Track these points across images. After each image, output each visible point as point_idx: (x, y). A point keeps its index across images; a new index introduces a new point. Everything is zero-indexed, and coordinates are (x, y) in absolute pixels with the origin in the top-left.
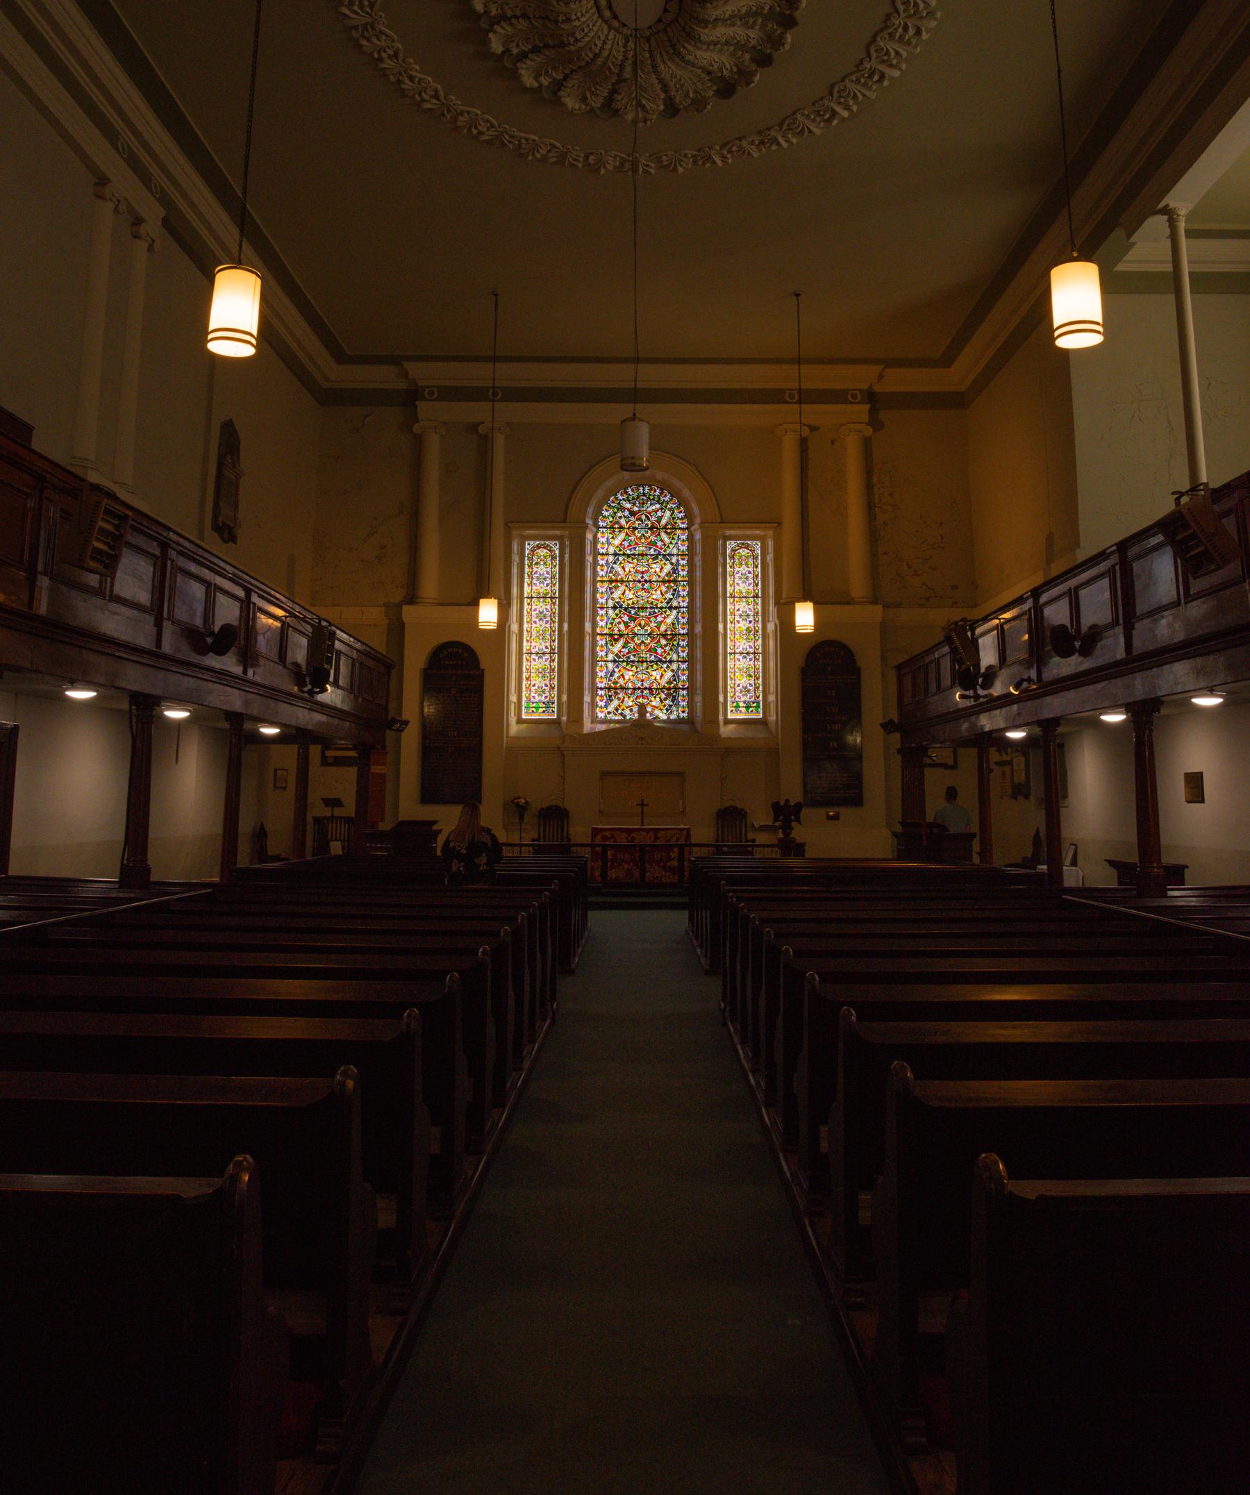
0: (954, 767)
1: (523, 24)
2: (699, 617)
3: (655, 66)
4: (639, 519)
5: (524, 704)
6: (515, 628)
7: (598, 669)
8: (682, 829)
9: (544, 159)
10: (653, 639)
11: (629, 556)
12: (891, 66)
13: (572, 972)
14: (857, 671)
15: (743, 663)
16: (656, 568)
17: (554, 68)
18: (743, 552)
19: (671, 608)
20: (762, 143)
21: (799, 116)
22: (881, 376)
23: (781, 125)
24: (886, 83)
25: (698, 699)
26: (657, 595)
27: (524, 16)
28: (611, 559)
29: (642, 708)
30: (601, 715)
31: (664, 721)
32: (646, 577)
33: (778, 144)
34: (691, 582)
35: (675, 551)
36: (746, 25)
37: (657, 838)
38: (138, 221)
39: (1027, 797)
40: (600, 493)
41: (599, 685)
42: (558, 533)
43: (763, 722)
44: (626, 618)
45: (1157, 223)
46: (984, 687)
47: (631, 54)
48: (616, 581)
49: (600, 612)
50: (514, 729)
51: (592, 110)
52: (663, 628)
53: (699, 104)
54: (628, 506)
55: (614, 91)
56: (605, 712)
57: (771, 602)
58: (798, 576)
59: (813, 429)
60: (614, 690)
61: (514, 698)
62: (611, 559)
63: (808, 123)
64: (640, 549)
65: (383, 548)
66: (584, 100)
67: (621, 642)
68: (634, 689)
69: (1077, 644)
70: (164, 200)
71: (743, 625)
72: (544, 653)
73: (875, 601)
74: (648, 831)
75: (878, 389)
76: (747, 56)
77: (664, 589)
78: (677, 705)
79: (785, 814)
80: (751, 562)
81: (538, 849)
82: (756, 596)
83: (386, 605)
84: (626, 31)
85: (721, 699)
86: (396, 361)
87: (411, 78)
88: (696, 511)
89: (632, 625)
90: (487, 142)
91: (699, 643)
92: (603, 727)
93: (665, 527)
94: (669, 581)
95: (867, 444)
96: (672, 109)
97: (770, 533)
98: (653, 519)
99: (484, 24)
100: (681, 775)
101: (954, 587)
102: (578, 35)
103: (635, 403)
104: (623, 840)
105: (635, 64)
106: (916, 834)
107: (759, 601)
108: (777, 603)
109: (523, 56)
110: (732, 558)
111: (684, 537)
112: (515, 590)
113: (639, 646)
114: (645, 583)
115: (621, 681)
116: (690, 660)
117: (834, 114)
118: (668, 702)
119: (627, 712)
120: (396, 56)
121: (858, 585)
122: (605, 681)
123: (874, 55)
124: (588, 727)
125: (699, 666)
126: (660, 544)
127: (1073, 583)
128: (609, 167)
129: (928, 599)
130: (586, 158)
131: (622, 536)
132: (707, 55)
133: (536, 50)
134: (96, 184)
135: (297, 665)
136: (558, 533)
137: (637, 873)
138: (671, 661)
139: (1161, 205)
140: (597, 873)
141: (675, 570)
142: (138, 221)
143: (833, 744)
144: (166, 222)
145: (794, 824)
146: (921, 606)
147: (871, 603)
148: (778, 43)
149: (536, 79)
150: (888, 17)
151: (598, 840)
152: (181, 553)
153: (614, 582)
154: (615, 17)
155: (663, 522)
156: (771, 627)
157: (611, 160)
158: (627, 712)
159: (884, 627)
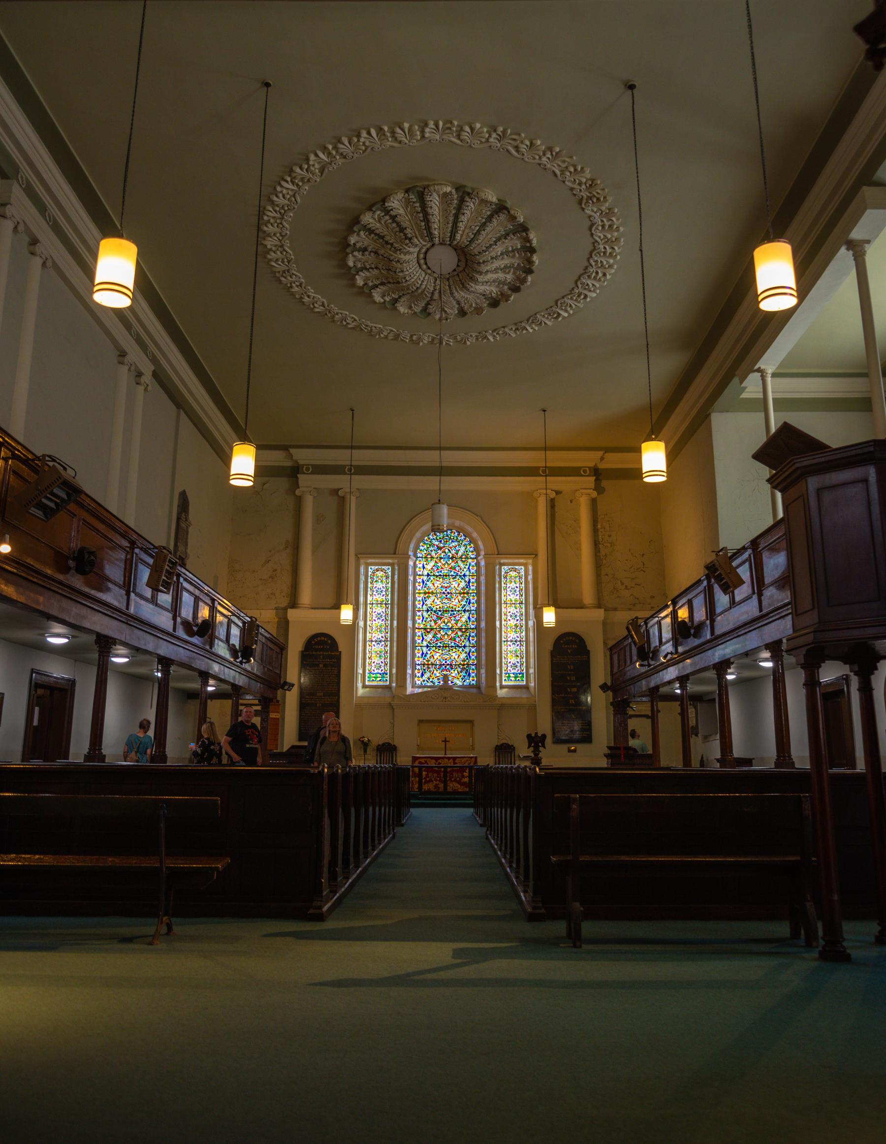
1: (376, 272)
2: (483, 616)
3: (452, 294)
4: (444, 552)
6: (361, 624)
9: (386, 337)
10: (453, 631)
12: (590, 291)
13: (402, 825)
15: (513, 648)
16: (455, 584)
17: (393, 292)
18: (513, 574)
20: (517, 329)
21: (538, 316)
22: (602, 459)
23: (528, 320)
24: (588, 299)
25: (483, 671)
27: (376, 268)
28: (425, 578)
29: (446, 678)
30: (418, 682)
31: (460, 686)
34: (478, 594)
36: (504, 272)
38: (139, 375)
40: (418, 535)
41: (417, 662)
42: (390, 561)
43: (526, 687)
45: (754, 377)
46: (652, 659)
47: (438, 287)
48: (429, 593)
49: (418, 614)
50: (361, 691)
51: (415, 313)
52: (459, 625)
53: (479, 310)
54: (437, 543)
55: (428, 304)
56: (419, 682)
57: (531, 607)
58: (553, 589)
59: (558, 493)
60: (427, 666)
61: (360, 671)
63: (544, 319)
64: (445, 572)
65: (275, 570)
66: (410, 308)
67: (432, 633)
68: (441, 665)
69: (692, 631)
70: (154, 360)
71: (513, 622)
73: (599, 606)
74: (449, 758)
75: (601, 466)
76: (506, 287)
77: (460, 598)
78: (469, 675)
79: (536, 741)
83: (276, 609)
84: (435, 275)
85: (498, 671)
86: (285, 448)
87: (309, 296)
88: (482, 547)
89: (439, 622)
90: (353, 328)
91: (483, 634)
92: (420, 690)
93: (461, 557)
94: (464, 593)
95: (594, 503)
96: (462, 313)
97: (530, 561)
98: (453, 552)
99: (353, 271)
101: (652, 597)
102: (407, 278)
103: (440, 475)
104: (432, 763)
105: (440, 292)
106: (620, 752)
107: (523, 606)
108: (535, 608)
109: (375, 287)
110: (505, 578)
111: (473, 564)
112: (362, 599)
113: (444, 636)
114: (447, 594)
115: (432, 660)
116: (478, 646)
117: (559, 315)
118: (463, 674)
119: (436, 680)
120: (301, 285)
121: (588, 595)
122: (421, 659)
123: (580, 286)
124: (409, 690)
125: (483, 650)
126: (457, 569)
127: (690, 596)
129: (634, 605)
130: (411, 336)
131: (432, 563)
132: (482, 288)
133: (383, 284)
134: (120, 356)
135: (234, 645)
136: (390, 561)
137: (441, 785)
138: (465, 646)
139: (756, 367)
140: (416, 786)
141: (468, 586)
142: (139, 375)
143: (572, 701)
144: (155, 375)
145: (541, 749)
146: (630, 609)
147: (595, 607)
148: (524, 281)
149: (382, 297)
151: (416, 764)
152: (185, 580)
154: (429, 268)
155: (460, 554)
156: (531, 623)
157: (426, 338)
158: (436, 680)
159: (605, 624)
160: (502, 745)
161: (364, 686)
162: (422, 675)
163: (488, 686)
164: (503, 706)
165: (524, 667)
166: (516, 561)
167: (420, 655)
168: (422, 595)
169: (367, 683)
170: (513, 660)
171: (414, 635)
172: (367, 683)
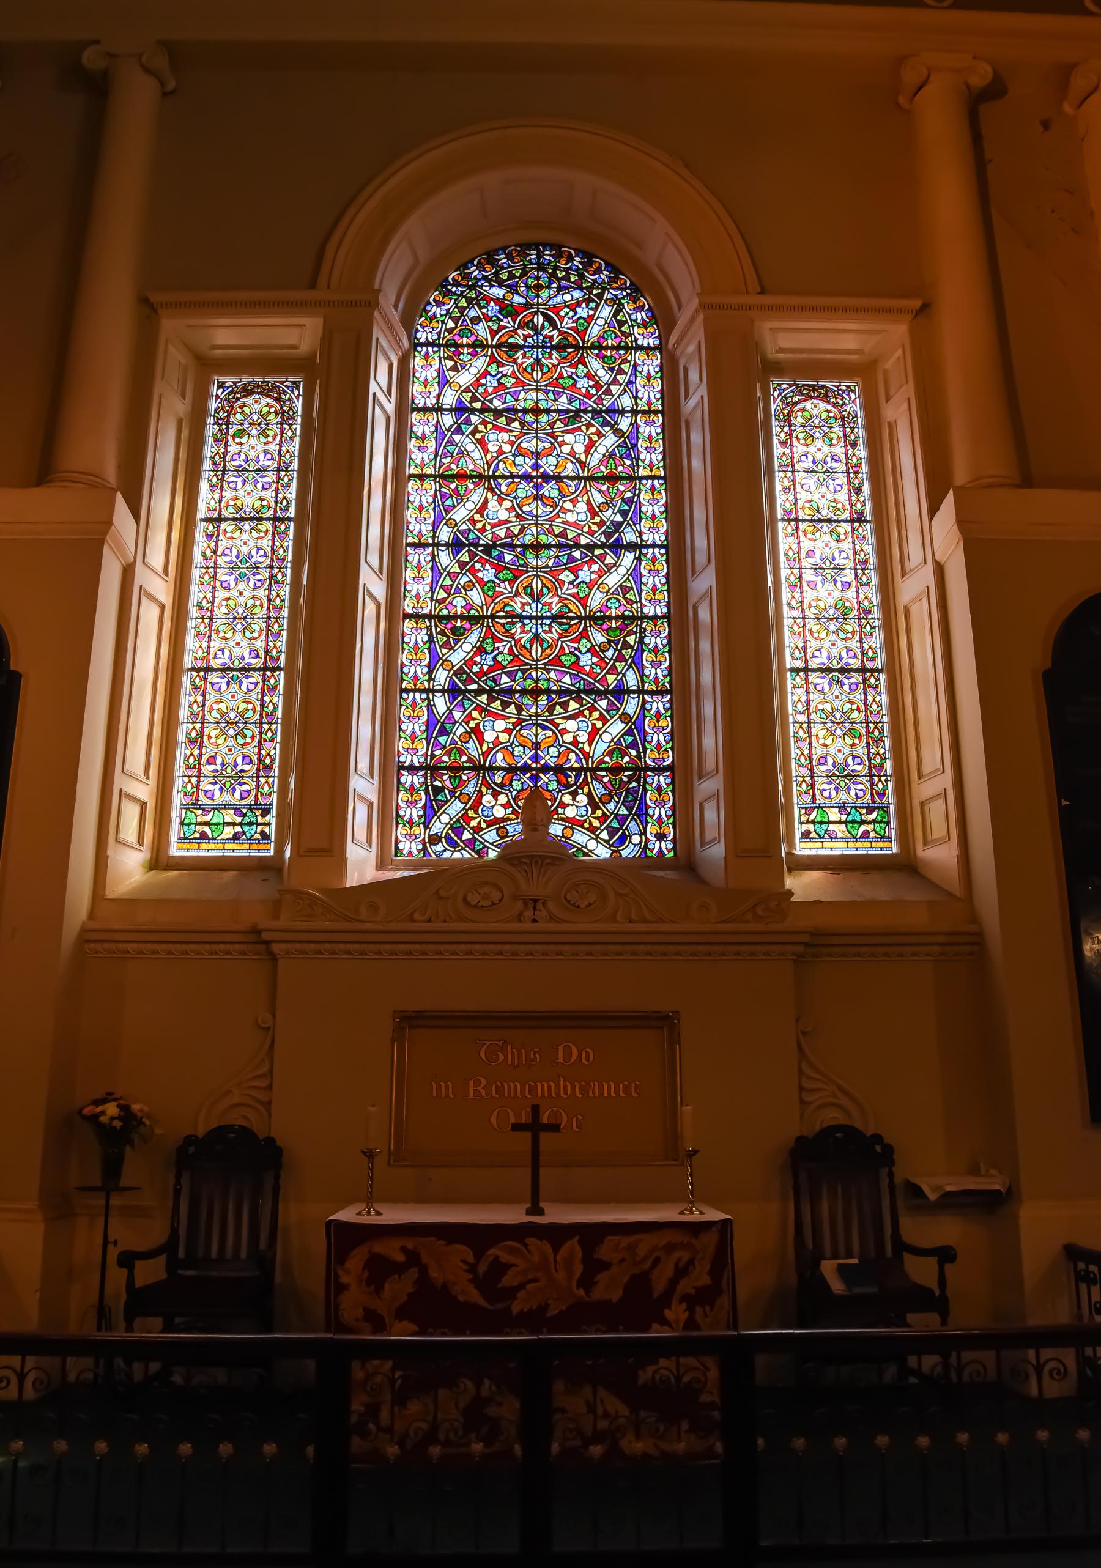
4: (528, 324)
7: (403, 712)
8: (708, 1225)
11: (498, 414)
15: (830, 698)
16: (575, 442)
18: (816, 408)
19: (617, 547)
28: (448, 420)
35: (626, 402)
37: (594, 1267)
41: (406, 759)
48: (462, 476)
49: (414, 556)
62: (448, 420)
64: (526, 400)
72: (246, 670)
74: (558, 1234)
78: (642, 814)
80: (837, 432)
82: (860, 519)
100: (664, 1023)
107: (867, 530)
110: (788, 420)
115: (472, 748)
125: (710, 710)
126: (583, 383)
153: (451, 480)
155: (595, 331)
160: (830, 1131)
161: (159, 861)
162: (430, 813)
163: (737, 851)
167: (419, 727)
168: (431, 486)
169: (175, 850)
171: (392, 645)
172: (175, 850)
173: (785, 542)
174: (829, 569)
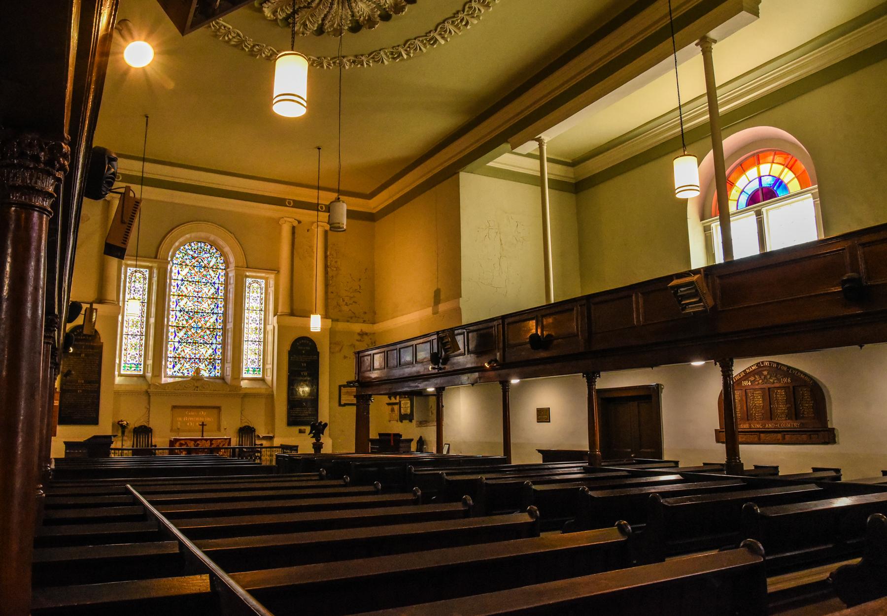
0: (340, 405)
5: (123, 365)
14: (318, 354)
15: (254, 347)
16: (205, 290)
18: (255, 285)
20: (354, 62)
21: (382, 53)
23: (369, 55)
26: (205, 305)
28: (180, 282)
29: (198, 371)
32: (200, 295)
33: (362, 65)
34: (226, 299)
37: (211, 444)
39: (411, 421)
42: (150, 265)
44: (187, 317)
50: (118, 380)
52: (208, 324)
56: (171, 373)
59: (299, 222)
60: (178, 359)
63: (384, 56)
64: (197, 279)
67: (184, 330)
68: (190, 359)
71: (254, 326)
76: (379, 13)
81: (135, 452)
85: (117, 361)
89: (190, 321)
96: (320, 31)
97: (273, 276)
98: (206, 262)
101: (365, 313)
104: (192, 445)
107: (263, 313)
116: (224, 344)
119: (185, 371)
124: (164, 380)
128: (263, 55)
130: (254, 46)
131: (186, 270)
146: (348, 321)
150: (458, 12)
155: (211, 264)
158: (185, 371)
162: (174, 366)
164: (246, 396)
165: (261, 363)
166: (259, 275)
170: (253, 357)
173: (246, 315)
174: (254, 320)
